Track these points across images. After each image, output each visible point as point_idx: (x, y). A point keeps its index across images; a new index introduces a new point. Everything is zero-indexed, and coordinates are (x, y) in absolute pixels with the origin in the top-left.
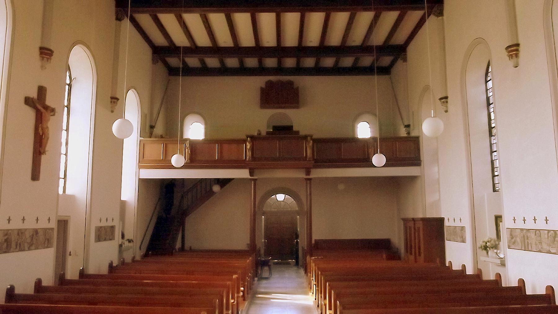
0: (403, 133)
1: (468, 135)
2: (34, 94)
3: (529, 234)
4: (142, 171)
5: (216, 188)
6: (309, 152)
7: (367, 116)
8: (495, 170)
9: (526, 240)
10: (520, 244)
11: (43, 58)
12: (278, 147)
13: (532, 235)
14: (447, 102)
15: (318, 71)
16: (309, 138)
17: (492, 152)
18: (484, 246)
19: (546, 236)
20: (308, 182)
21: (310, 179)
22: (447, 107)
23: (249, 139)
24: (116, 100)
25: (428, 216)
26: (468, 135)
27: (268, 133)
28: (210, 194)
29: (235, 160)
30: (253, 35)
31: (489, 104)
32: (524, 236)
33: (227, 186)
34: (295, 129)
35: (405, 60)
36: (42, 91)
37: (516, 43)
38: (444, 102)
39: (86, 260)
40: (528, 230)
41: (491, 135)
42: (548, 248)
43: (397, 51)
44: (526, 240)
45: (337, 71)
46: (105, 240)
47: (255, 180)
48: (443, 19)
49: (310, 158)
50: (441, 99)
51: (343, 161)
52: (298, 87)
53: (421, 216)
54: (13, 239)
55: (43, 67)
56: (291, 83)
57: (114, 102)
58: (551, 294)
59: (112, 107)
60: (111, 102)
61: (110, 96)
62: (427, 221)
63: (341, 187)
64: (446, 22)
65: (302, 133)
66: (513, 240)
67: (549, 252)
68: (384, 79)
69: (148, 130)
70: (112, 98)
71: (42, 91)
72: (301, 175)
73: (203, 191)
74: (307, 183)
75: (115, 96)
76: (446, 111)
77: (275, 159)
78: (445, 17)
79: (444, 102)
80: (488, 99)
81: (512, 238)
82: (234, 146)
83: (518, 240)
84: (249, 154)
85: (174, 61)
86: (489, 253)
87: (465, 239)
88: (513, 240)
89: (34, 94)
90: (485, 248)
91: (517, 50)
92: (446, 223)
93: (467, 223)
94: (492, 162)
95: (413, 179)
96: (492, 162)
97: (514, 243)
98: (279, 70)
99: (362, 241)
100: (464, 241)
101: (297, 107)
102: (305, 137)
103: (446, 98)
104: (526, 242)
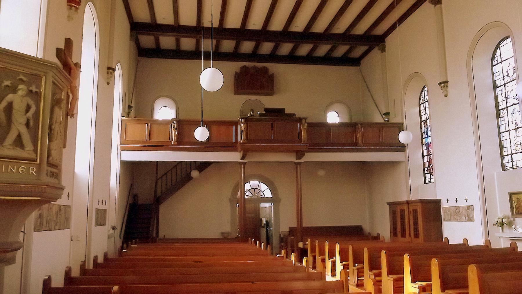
0: (379, 119)
1: (476, 117)
2: (62, 46)
4: (123, 152)
5: (195, 174)
8: (505, 149)
11: (71, 6)
14: (447, 86)
15: (292, 59)
16: (303, 121)
17: (500, 133)
18: (500, 223)
20: (299, 166)
21: (300, 163)
22: (447, 91)
24: (112, 71)
25: (413, 199)
26: (476, 117)
27: (261, 115)
29: (222, 143)
33: (208, 169)
35: (383, 50)
36: (68, 42)
38: (444, 87)
39: (88, 244)
41: (498, 117)
43: (375, 40)
45: (310, 59)
46: (55, 229)
47: (245, 163)
49: (304, 141)
50: (440, 84)
51: (333, 145)
52: (273, 74)
53: (405, 199)
54: (44, 215)
55: (69, 18)
56: (266, 70)
57: (111, 73)
59: (108, 78)
60: (108, 73)
61: (106, 65)
62: (424, 202)
64: (443, 9)
65: (298, 116)
68: (351, 70)
69: (128, 110)
70: (109, 68)
71: (68, 42)
72: (291, 158)
73: (179, 177)
74: (296, 168)
75: (111, 66)
76: (446, 96)
77: (270, 141)
78: (443, 5)
79: (444, 87)
80: (495, 82)
82: (223, 128)
84: (243, 135)
85: (147, 41)
86: (504, 230)
89: (62, 46)
90: (502, 224)
92: (444, 204)
93: (476, 202)
95: (393, 164)
98: (254, 56)
99: (327, 228)
100: (471, 219)
101: (271, 94)
102: (300, 120)
103: (447, 82)
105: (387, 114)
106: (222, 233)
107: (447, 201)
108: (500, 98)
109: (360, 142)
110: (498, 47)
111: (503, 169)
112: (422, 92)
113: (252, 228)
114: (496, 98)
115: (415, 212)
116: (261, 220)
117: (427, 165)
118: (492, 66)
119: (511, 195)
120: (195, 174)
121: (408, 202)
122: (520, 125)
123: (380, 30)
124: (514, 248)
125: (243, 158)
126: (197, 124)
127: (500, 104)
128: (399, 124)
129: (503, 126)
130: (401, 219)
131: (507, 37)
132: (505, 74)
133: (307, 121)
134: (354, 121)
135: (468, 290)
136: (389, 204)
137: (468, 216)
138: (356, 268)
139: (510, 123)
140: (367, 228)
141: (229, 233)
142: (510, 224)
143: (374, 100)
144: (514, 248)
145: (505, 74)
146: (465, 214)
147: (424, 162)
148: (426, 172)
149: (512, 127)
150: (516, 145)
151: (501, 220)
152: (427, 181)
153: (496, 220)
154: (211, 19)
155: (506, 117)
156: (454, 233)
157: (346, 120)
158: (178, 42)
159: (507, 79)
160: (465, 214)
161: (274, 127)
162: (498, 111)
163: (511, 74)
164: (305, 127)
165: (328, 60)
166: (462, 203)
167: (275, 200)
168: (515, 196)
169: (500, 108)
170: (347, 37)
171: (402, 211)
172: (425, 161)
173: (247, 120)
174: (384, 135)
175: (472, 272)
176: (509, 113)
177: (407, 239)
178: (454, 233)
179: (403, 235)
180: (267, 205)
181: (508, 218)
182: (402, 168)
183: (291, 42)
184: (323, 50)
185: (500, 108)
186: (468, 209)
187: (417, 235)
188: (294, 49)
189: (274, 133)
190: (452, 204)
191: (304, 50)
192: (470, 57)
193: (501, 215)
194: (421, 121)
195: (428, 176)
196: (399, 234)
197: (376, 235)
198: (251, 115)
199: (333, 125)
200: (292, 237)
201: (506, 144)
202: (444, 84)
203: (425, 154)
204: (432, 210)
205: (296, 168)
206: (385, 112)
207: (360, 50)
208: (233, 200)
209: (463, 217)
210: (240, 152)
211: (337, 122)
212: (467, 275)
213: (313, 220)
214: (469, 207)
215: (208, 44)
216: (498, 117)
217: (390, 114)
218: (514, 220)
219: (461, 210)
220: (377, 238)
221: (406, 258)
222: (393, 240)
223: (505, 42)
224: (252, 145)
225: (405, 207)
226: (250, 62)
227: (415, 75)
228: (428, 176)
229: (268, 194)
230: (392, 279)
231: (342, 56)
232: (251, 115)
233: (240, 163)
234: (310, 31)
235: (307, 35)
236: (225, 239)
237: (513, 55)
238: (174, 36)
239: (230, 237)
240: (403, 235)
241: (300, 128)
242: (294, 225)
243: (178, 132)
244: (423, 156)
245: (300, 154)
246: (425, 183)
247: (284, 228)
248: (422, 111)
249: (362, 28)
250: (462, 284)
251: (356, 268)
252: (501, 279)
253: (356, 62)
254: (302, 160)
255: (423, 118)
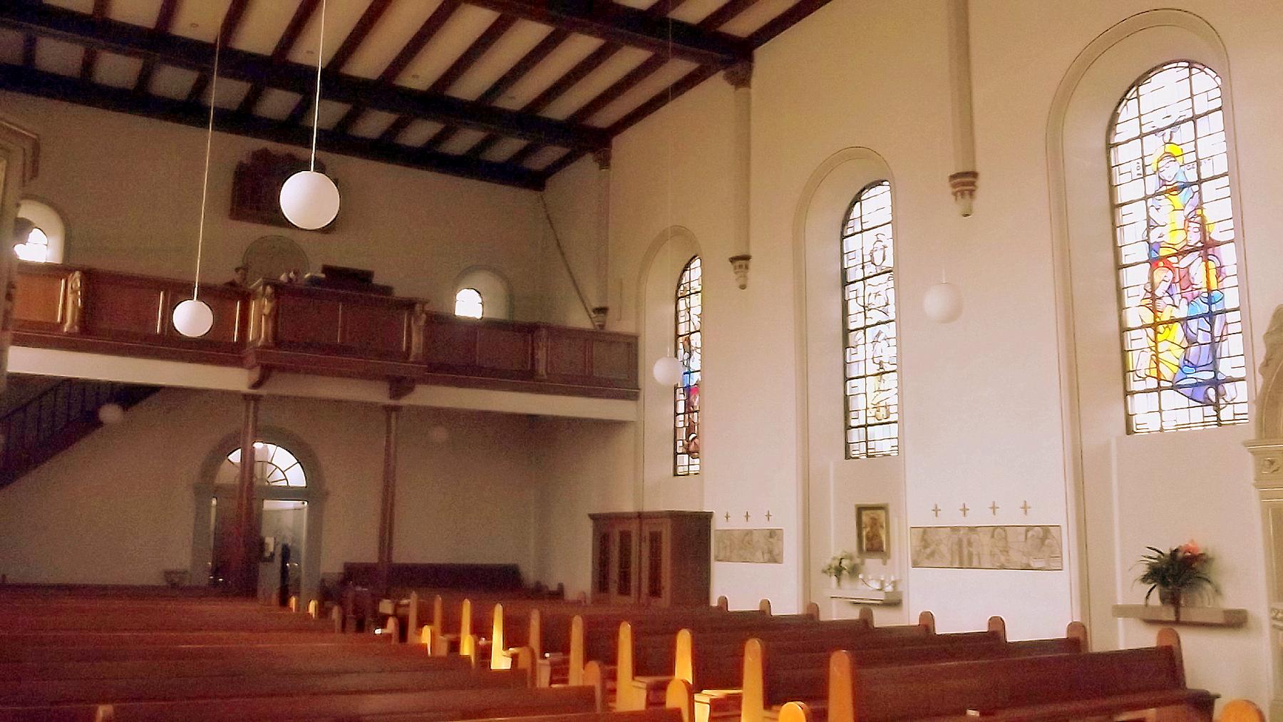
0: (579, 319)
3: (974, 537)
5: (110, 413)
6: (417, 340)
7: (482, 278)
8: (853, 415)
9: (961, 548)
10: (948, 556)
12: (336, 322)
13: (985, 538)
14: (747, 267)
16: (418, 308)
19: (1022, 538)
20: (394, 415)
21: (396, 409)
23: (269, 289)
25: (649, 506)
27: (314, 281)
28: (91, 422)
30: (398, 50)
31: (845, 283)
32: (960, 541)
34: (378, 280)
35: (605, 162)
37: (969, 169)
40: (972, 529)
42: (1025, 560)
43: (589, 138)
44: (961, 548)
45: (428, 158)
48: (749, 94)
49: (416, 356)
50: (733, 260)
53: (628, 507)
58: (1082, 638)
63: (439, 434)
64: (754, 98)
65: (400, 292)
66: (928, 551)
67: (1028, 568)
72: (377, 394)
76: (743, 287)
79: (740, 266)
80: (844, 272)
81: (925, 547)
83: (944, 549)
86: (842, 583)
87: (781, 554)
88: (928, 551)
90: (839, 571)
91: (973, 184)
92: (718, 524)
94: (846, 398)
95: (608, 427)
96: (846, 398)
97: (932, 554)
100: (774, 558)
103: (747, 258)
104: (965, 552)
105: (602, 310)
106: (168, 574)
107: (768, 516)
108: (853, 307)
109: (541, 369)
110: (857, 199)
111: (848, 456)
112: (684, 270)
113: (240, 560)
114: (845, 305)
115: (655, 539)
116: (262, 544)
117: (682, 434)
118: (843, 237)
119: (860, 510)
120: (110, 413)
121: (640, 516)
122: (888, 368)
123: (603, 119)
124: (866, 621)
125: (257, 385)
126: (179, 291)
127: (851, 318)
128: (627, 336)
129: (854, 366)
130: (621, 551)
131: (879, 183)
132: (867, 258)
133: (427, 308)
134: (521, 318)
135: (827, 703)
136: (593, 517)
137: (770, 552)
138: (547, 662)
139: (869, 362)
140: (530, 574)
141: (185, 572)
142: (854, 571)
143: (572, 277)
144: (866, 621)
145: (867, 258)
146: (764, 546)
147: (675, 428)
148: (679, 450)
149: (873, 369)
150: (876, 407)
151: (837, 563)
152: (680, 470)
153: (829, 561)
154: (259, 35)
155: (861, 349)
156: (736, 586)
157: (499, 314)
158: (30, 44)
159: (870, 270)
160: (764, 546)
161: (344, 313)
162: (846, 332)
163: (878, 261)
164: (422, 323)
165: (470, 166)
166: (758, 523)
167: (312, 493)
168: (868, 512)
169: (852, 327)
170: (529, 121)
171: (625, 537)
172: (680, 424)
173: (280, 291)
174: (608, 363)
175: (840, 667)
176: (869, 339)
177: (631, 599)
178: (736, 586)
179: (624, 589)
180: (290, 504)
181: (851, 558)
182: (627, 437)
183: (392, 111)
184: (464, 140)
185: (852, 327)
186: (771, 536)
187: (655, 591)
188: (397, 127)
189: (344, 331)
190: (738, 524)
191: (420, 133)
192: (803, 209)
193: (839, 554)
194: (677, 336)
195: (683, 460)
196: (614, 588)
197: (553, 587)
198: (290, 280)
199: (471, 326)
200: (359, 589)
201: (858, 403)
202: (741, 260)
203: (681, 409)
204: (693, 532)
205: (389, 419)
206: (597, 306)
207: (553, 153)
208: (206, 486)
209: (759, 554)
210: (251, 368)
211: (479, 316)
212: (828, 673)
213: (415, 547)
214: (772, 533)
215: (224, 92)
216: (846, 345)
217: (610, 312)
218: (863, 563)
219: (756, 537)
220: (559, 594)
221: (684, 641)
222: (596, 602)
223: (873, 191)
224: (290, 351)
225: (633, 527)
226: (278, 141)
227: (679, 232)
228: (683, 460)
229: (297, 477)
230: (644, 686)
231: (509, 162)
232: (290, 280)
233: (246, 397)
234: (494, 104)
235: (436, 102)
236: (174, 587)
237: (890, 219)
238: (82, 42)
239: (187, 583)
240: (624, 589)
241: (409, 320)
242: (368, 553)
243: (85, 299)
244: (676, 414)
245: (400, 386)
246: (676, 475)
247: (331, 566)
248: (682, 313)
249: (562, 109)
250: (815, 694)
251: (547, 662)
252: (891, 683)
253: (536, 181)
254: (404, 402)
255: (682, 330)
